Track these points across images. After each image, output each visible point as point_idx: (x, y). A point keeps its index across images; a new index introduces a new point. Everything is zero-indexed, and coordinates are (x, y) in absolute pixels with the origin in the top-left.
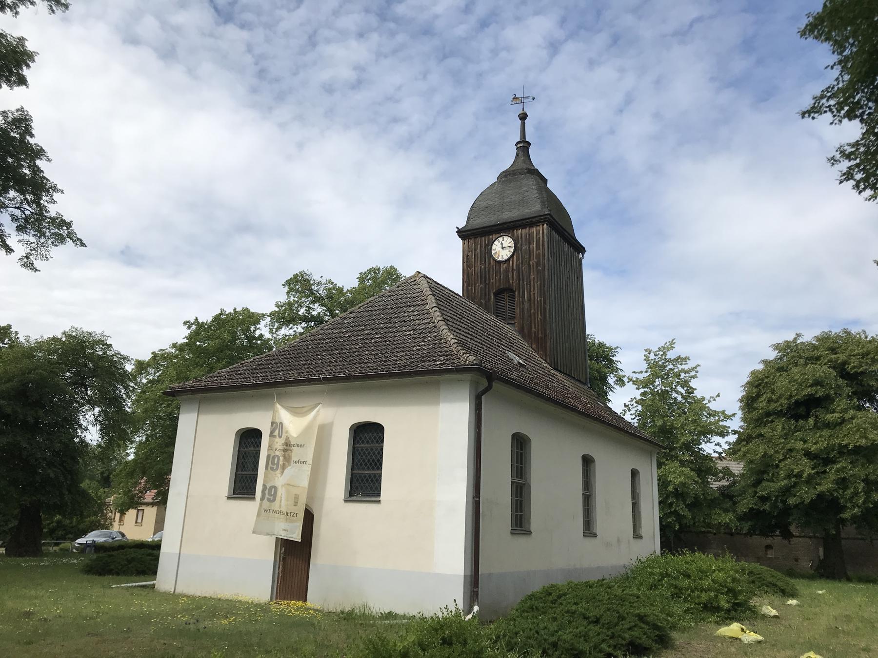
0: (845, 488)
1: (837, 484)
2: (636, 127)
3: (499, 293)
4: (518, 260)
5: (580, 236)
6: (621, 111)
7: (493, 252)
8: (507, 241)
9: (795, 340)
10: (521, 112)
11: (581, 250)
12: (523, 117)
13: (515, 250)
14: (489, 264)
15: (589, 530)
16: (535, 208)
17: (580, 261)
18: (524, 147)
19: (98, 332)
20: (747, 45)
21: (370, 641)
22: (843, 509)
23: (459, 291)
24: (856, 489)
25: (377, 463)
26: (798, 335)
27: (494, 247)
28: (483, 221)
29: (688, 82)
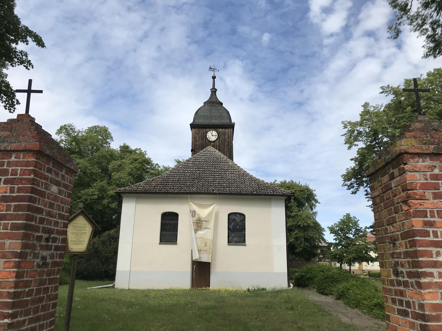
0: (297, 241)
1: (295, 239)
2: (147, 52)
4: (219, 142)
6: (141, 40)
7: (207, 136)
8: (214, 133)
9: (274, 182)
10: (213, 75)
12: (214, 78)
13: (218, 137)
14: (205, 141)
18: (214, 91)
20: (206, 25)
22: (296, 248)
24: (301, 241)
26: (275, 181)
27: (208, 134)
28: (200, 121)
29: (176, 36)
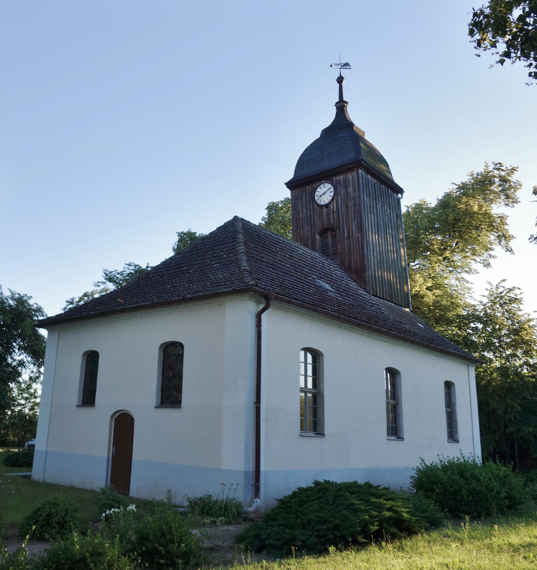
3: (323, 233)
5: (398, 179)
11: (399, 190)
13: (334, 194)
15: (394, 429)
16: (348, 156)
17: (399, 200)
18: (341, 106)
19: (443, 195)
21: (523, 503)
23: (404, 210)
25: (179, 376)
